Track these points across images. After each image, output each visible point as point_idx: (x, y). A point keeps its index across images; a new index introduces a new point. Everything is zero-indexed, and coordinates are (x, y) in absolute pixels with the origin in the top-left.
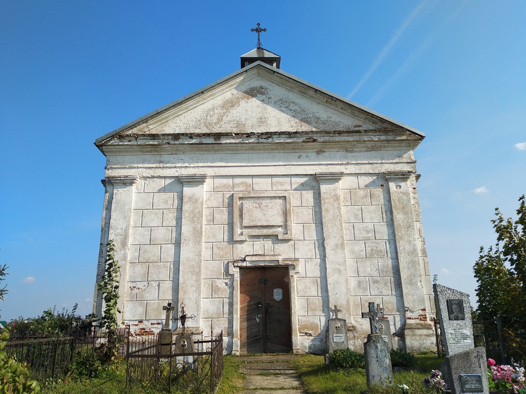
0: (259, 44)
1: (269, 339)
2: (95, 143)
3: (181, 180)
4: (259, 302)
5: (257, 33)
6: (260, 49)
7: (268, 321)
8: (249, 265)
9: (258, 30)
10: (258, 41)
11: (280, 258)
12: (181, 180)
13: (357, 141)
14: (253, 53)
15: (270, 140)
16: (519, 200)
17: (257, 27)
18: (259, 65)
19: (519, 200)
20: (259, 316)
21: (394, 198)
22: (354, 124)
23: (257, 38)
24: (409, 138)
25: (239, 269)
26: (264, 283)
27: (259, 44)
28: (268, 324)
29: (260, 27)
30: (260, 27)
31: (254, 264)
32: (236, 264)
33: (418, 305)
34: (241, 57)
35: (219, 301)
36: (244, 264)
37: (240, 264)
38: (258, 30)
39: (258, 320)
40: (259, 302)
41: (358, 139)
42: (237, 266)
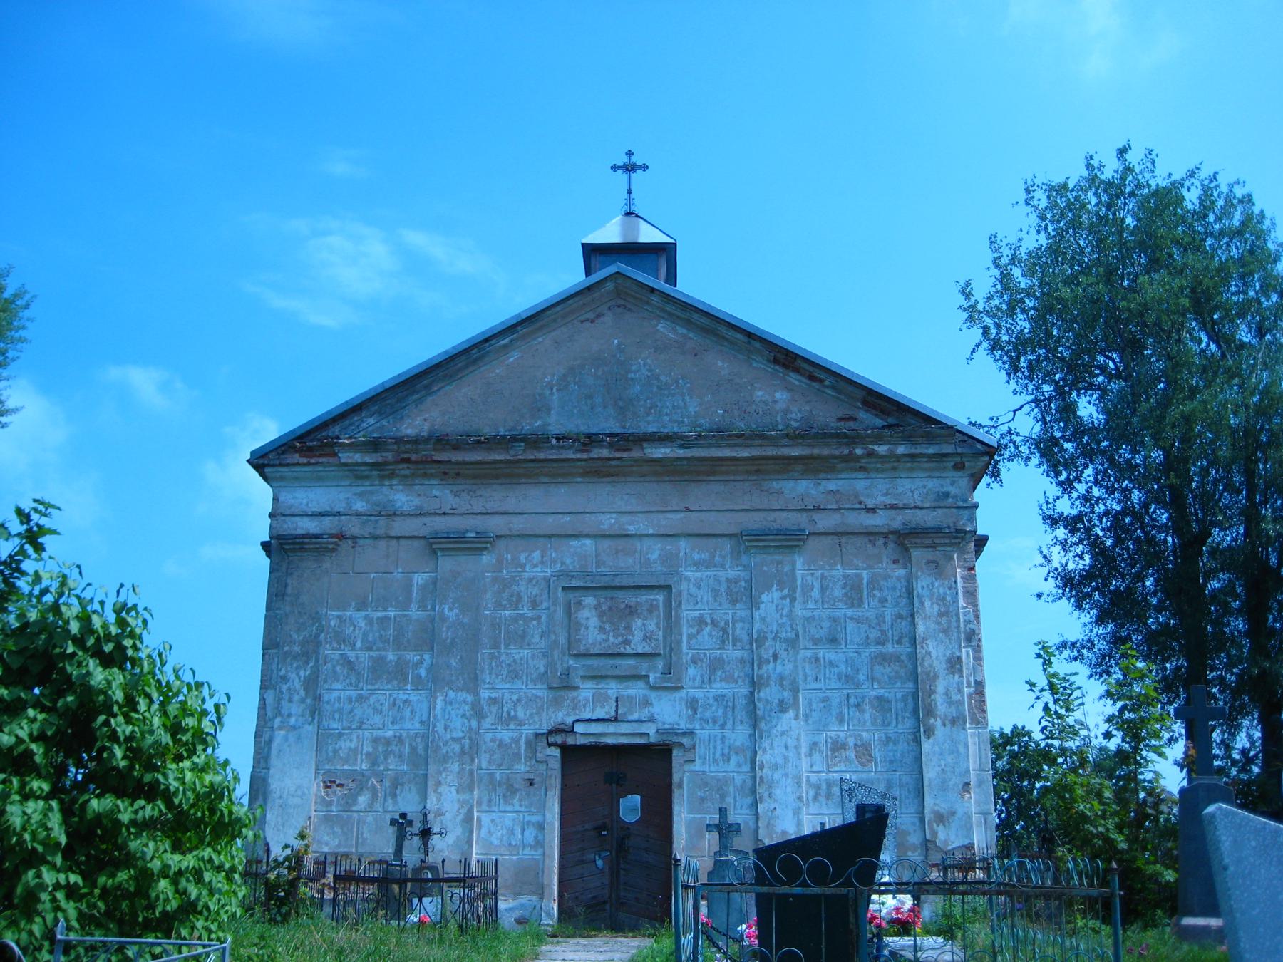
0: (630, 201)
1: (622, 904)
2: (248, 461)
3: (434, 546)
4: (604, 823)
5: (625, 176)
6: (633, 218)
7: (622, 866)
8: (581, 741)
9: (629, 168)
10: (626, 196)
11: (651, 729)
12: (434, 546)
13: (835, 457)
14: (610, 233)
15: (636, 453)
16: (35, 501)
17: (625, 159)
18: (618, 273)
19: (35, 501)
20: (604, 854)
21: (920, 591)
22: (840, 415)
23: (626, 187)
24: (959, 450)
25: (558, 751)
26: (618, 784)
27: (630, 201)
28: (622, 872)
29: (634, 159)
30: (634, 159)
31: (592, 740)
32: (551, 740)
33: (957, 836)
34: (583, 244)
35: (514, 820)
36: (570, 740)
37: (559, 739)
38: (629, 168)
39: (600, 863)
40: (604, 823)
41: (846, 452)
42: (555, 744)
